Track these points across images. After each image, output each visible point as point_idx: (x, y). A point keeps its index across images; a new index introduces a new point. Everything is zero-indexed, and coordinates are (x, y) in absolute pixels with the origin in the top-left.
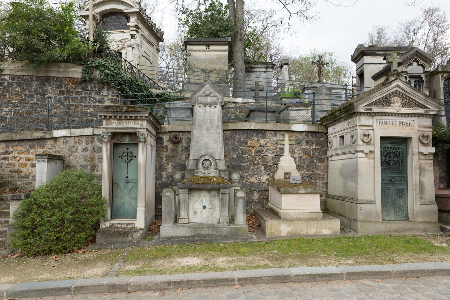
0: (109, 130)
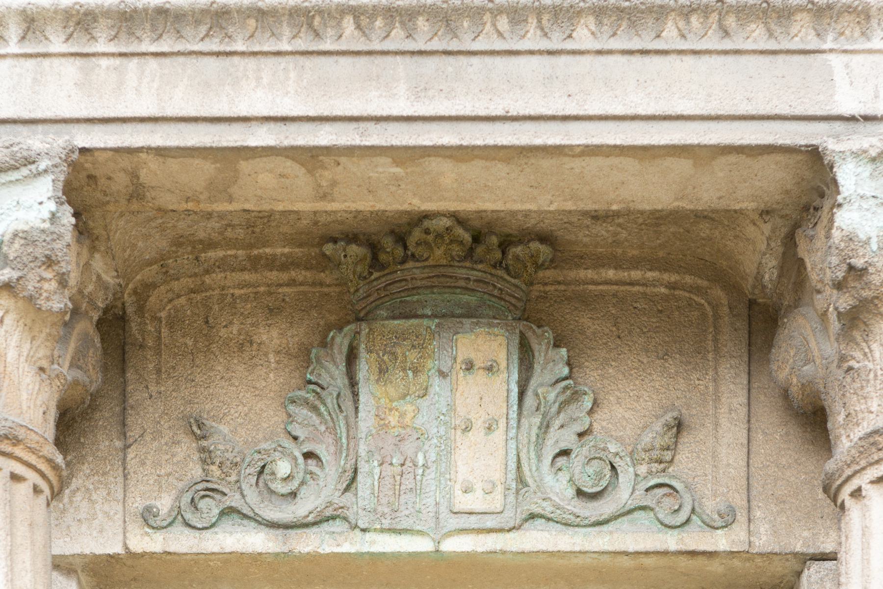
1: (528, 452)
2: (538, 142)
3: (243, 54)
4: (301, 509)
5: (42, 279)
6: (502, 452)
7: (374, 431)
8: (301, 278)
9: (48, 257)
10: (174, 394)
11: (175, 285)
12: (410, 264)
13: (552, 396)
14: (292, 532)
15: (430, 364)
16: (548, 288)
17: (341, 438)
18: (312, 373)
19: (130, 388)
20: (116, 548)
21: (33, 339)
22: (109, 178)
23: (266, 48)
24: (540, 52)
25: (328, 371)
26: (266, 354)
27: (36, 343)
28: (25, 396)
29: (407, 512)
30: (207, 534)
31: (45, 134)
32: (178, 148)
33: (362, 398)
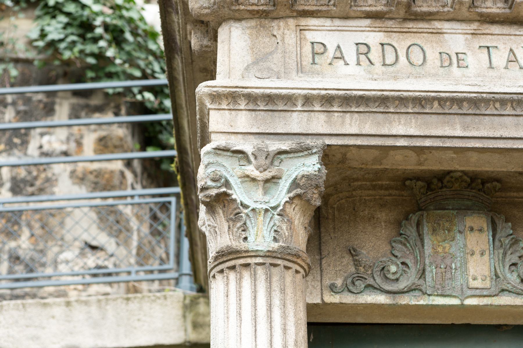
0: (296, 122)
1: (499, 264)
2: (515, 147)
3: (393, 113)
4: (402, 285)
5: (314, 193)
6: (488, 264)
7: (432, 254)
8: (394, 193)
9: (317, 185)
10: (341, 237)
11: (341, 195)
12: (444, 189)
13: (507, 241)
14: (397, 295)
15: (455, 228)
16: (498, 199)
17: (417, 257)
18: (402, 230)
19: (322, 235)
20: (319, 301)
21: (304, 216)
22: (334, 156)
23: (402, 111)
24: (512, 115)
25: (409, 230)
26: (380, 223)
27: (306, 217)
28: (301, 238)
29: (449, 288)
30: (359, 296)
31: (312, 139)
32: (368, 146)
33: (426, 241)
